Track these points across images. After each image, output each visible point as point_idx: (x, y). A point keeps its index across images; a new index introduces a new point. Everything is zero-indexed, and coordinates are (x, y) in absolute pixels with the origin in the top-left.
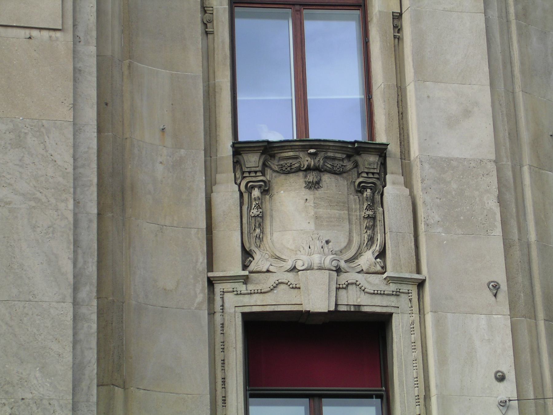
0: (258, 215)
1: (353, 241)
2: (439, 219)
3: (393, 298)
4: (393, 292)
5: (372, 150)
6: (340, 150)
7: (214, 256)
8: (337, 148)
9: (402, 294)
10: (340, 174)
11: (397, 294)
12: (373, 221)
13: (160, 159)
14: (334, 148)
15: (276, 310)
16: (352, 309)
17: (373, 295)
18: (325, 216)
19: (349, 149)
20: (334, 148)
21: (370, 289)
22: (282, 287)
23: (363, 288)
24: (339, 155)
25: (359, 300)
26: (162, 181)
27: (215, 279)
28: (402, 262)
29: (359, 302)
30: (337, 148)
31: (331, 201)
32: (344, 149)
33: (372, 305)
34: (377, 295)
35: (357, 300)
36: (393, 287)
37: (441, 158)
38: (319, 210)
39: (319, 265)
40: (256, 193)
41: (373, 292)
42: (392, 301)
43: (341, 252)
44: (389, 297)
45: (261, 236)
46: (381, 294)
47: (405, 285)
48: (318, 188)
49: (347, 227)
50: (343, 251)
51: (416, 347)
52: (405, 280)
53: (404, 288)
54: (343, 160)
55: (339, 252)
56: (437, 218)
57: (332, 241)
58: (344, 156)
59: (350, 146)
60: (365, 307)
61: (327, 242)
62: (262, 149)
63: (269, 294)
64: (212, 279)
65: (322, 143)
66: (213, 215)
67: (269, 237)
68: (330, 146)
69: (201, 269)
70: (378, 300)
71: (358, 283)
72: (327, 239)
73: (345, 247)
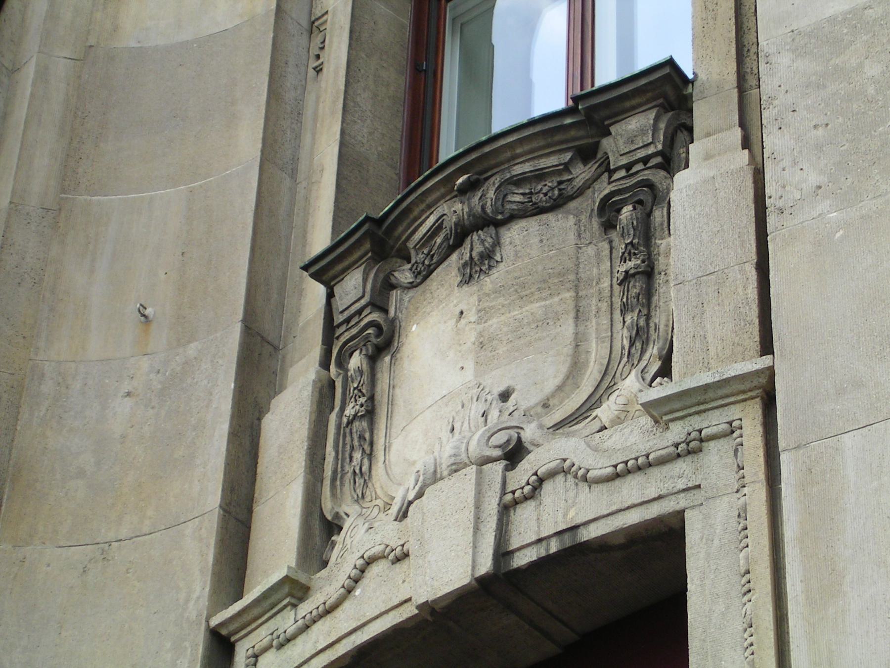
0: (355, 416)
1: (586, 364)
2: (822, 179)
3: (681, 466)
4: (677, 446)
5: (634, 102)
6: (548, 146)
7: (248, 572)
8: (535, 145)
9: (712, 444)
10: (557, 204)
11: (692, 448)
12: (643, 280)
13: (126, 387)
14: (527, 148)
15: (358, 642)
16: (554, 547)
17: (617, 482)
18: (505, 329)
19: (573, 133)
20: (527, 148)
21: (600, 467)
22: (376, 569)
23: (580, 473)
24: (553, 161)
25: (572, 514)
26: (123, 437)
27: (232, 627)
28: (712, 352)
29: (575, 516)
30: (535, 145)
31: (523, 286)
32: (558, 138)
33: (601, 512)
34: (630, 477)
35: (565, 515)
36: (677, 432)
37: (832, 20)
38: (490, 323)
39: (452, 460)
40: (356, 361)
41: (610, 470)
42: (681, 472)
43: (546, 406)
44: (666, 469)
45: (365, 468)
46: (639, 468)
47: (717, 412)
48: (490, 267)
49: (567, 328)
50: (551, 403)
51: (751, 585)
52: (711, 394)
53: (714, 422)
54: (567, 167)
55: (539, 409)
56: (813, 178)
57: (518, 387)
58: (568, 156)
59: (568, 121)
60: (592, 526)
61: (505, 396)
62: (367, 246)
63: (347, 605)
64: (224, 632)
65: (487, 149)
66: (259, 470)
67: (381, 459)
68: (510, 146)
69: (193, 616)
70: (631, 490)
71: (567, 464)
72: (502, 388)
73: (560, 388)
